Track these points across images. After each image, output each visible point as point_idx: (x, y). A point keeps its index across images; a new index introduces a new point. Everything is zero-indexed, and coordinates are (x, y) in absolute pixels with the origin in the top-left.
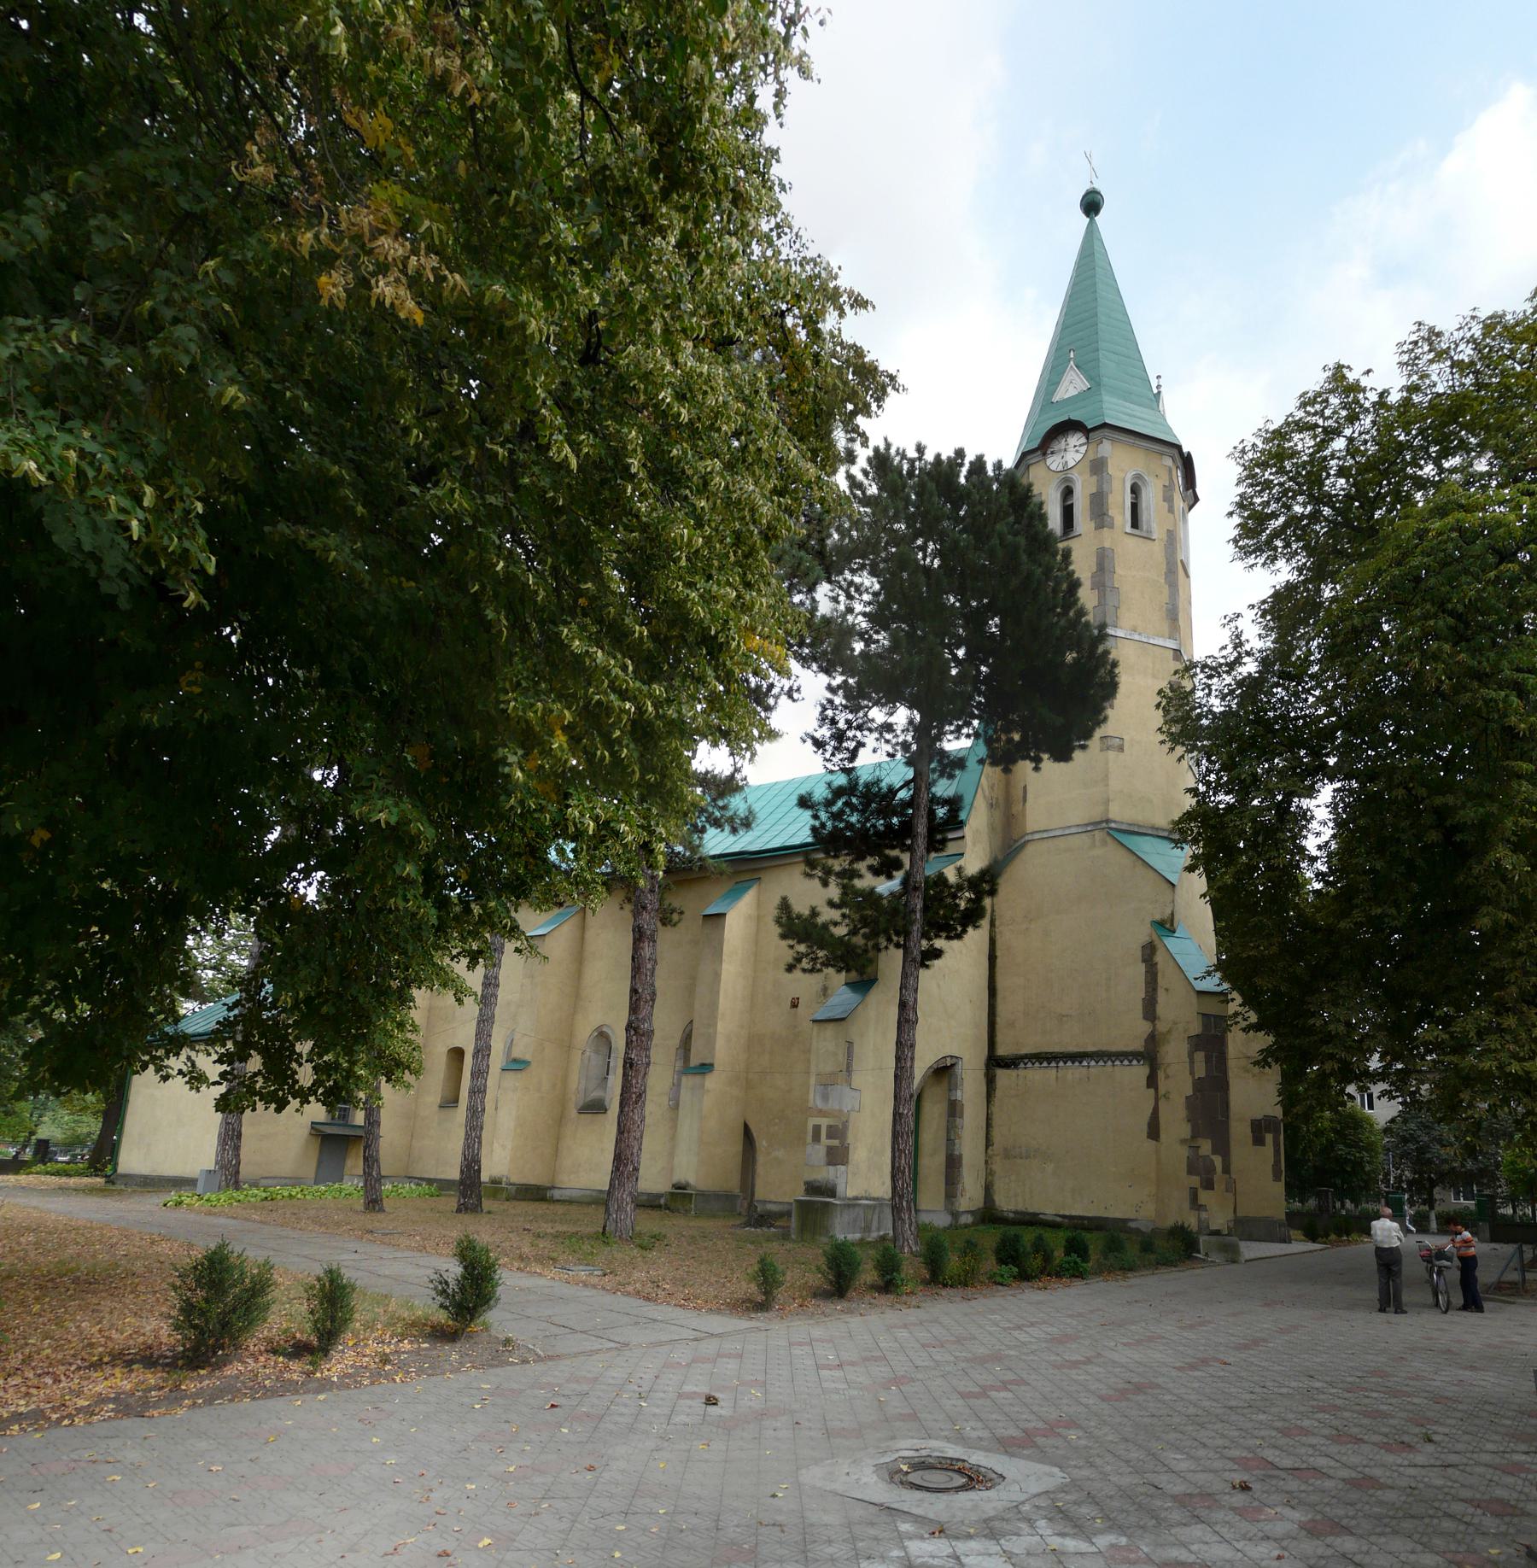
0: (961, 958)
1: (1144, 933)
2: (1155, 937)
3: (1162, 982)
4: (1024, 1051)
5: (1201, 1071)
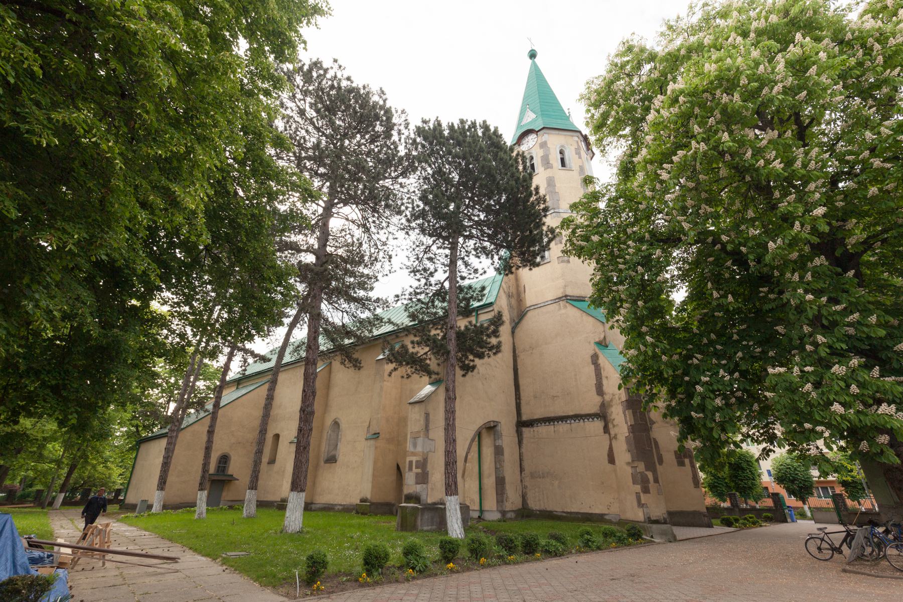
1: (591, 349)
3: (604, 374)
4: (536, 417)
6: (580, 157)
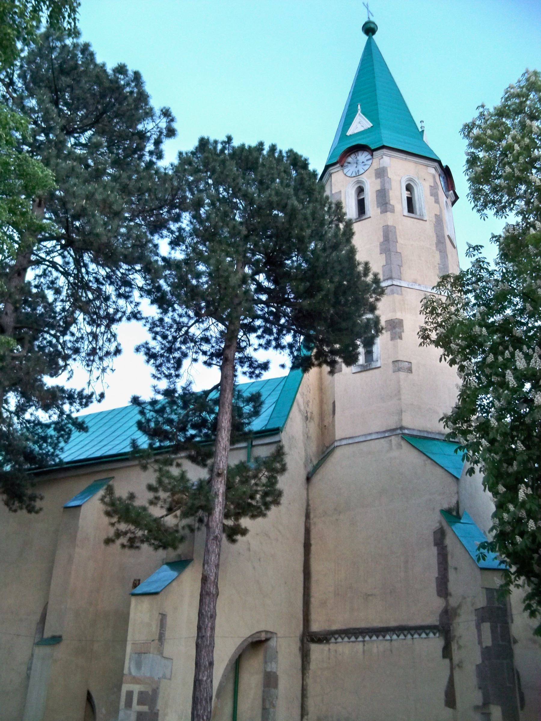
0: (270, 535)
1: (435, 520)
2: (445, 524)
3: (451, 562)
4: (334, 627)
5: (488, 642)
6: (437, 201)
